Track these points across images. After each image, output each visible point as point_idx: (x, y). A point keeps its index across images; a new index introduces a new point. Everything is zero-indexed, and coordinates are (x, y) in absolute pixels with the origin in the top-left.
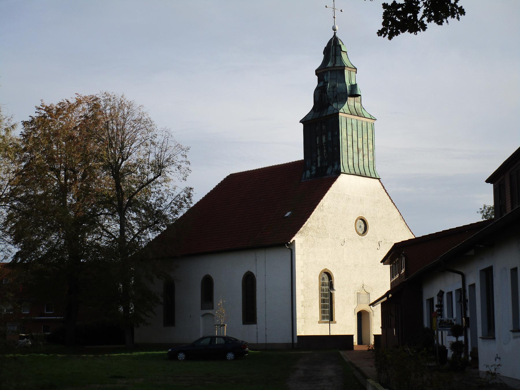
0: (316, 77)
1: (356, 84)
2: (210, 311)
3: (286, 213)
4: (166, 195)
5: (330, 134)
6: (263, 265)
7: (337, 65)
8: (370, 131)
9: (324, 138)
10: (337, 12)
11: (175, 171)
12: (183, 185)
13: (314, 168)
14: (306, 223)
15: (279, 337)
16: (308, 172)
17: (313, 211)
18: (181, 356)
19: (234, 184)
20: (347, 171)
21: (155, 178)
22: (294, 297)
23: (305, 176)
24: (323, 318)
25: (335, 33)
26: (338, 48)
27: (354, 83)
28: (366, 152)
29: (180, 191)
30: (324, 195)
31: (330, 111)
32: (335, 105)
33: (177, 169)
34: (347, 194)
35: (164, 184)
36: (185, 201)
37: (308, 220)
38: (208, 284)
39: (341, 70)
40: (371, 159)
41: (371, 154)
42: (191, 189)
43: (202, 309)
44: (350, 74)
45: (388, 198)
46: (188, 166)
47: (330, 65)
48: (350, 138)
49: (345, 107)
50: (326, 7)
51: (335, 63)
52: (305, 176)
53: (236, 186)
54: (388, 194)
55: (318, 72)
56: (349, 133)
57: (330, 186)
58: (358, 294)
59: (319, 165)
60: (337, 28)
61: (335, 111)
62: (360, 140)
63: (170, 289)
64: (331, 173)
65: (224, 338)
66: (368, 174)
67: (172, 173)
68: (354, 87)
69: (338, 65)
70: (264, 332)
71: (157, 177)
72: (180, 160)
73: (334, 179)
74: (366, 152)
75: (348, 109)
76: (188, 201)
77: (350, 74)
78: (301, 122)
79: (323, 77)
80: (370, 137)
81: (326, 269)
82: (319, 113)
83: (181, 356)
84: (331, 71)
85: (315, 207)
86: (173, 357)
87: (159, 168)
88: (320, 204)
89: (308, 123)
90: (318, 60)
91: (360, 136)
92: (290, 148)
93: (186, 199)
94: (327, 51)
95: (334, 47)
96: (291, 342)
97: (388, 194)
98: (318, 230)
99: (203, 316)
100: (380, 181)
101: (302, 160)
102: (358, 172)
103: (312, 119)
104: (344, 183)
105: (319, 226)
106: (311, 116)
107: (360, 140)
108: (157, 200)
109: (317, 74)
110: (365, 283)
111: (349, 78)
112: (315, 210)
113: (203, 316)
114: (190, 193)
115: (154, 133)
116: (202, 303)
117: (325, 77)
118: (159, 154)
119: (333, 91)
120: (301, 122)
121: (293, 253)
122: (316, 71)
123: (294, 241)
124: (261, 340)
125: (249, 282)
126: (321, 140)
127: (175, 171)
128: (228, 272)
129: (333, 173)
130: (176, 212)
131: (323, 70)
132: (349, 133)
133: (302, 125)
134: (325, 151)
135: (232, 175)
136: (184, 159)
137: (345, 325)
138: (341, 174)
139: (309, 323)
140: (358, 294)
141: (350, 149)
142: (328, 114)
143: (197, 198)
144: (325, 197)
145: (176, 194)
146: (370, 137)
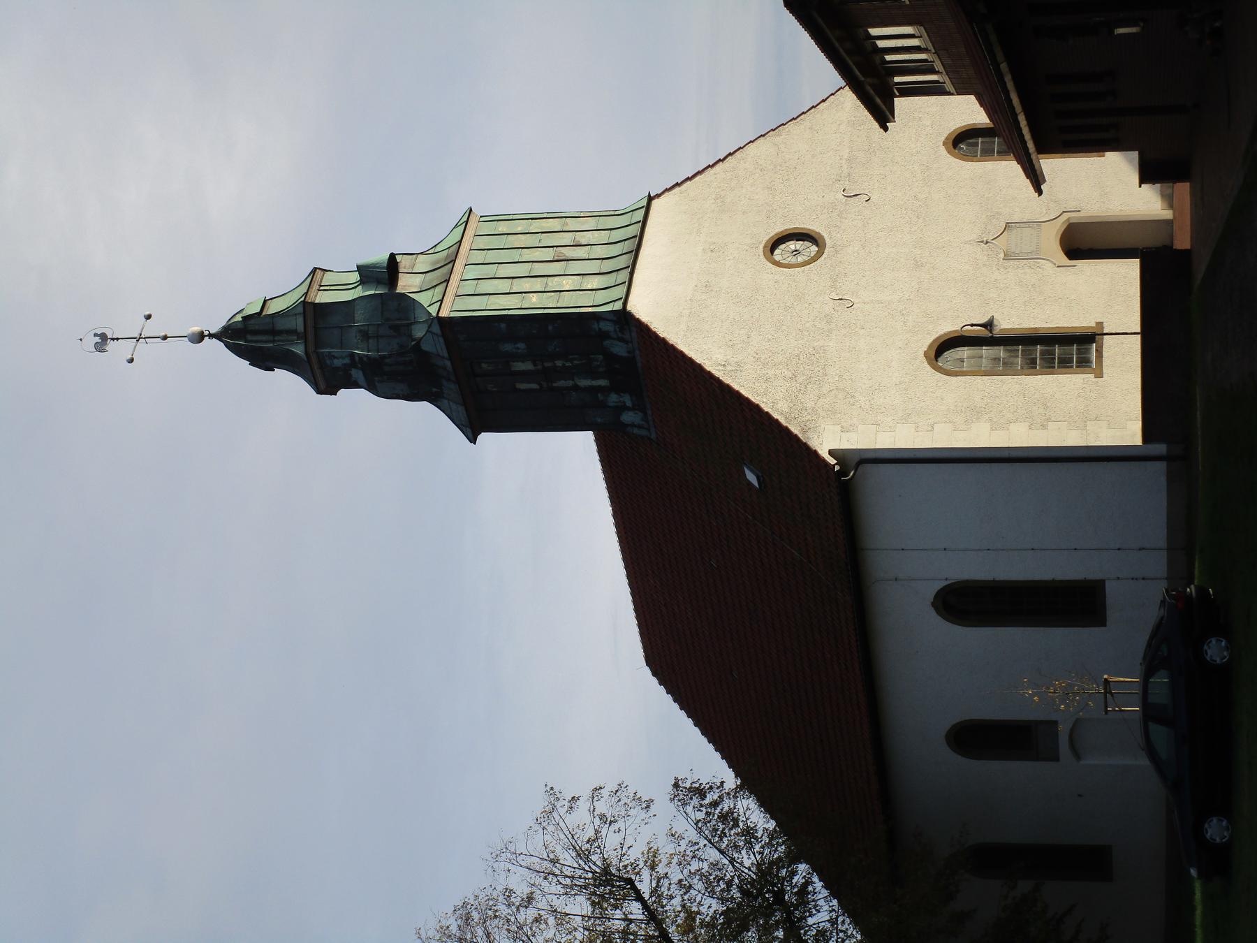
0: (342, 392)
2: (1063, 729)
3: (749, 483)
4: (695, 866)
5: (508, 347)
6: (913, 555)
7: (301, 328)
10: (152, 328)
11: (622, 834)
12: (665, 808)
13: (613, 398)
14: (776, 416)
15: (1149, 497)
16: (628, 417)
17: (738, 395)
18: (1215, 830)
19: (675, 650)
20: (620, 292)
21: (639, 898)
22: (1014, 454)
23: (640, 427)
24: (1084, 363)
25: (211, 336)
26: (253, 325)
27: (355, 277)
28: (567, 239)
29: (681, 819)
30: (690, 361)
31: (435, 346)
32: (419, 332)
33: (615, 826)
34: (695, 298)
35: (661, 869)
36: (715, 804)
37: (766, 408)
38: (975, 738)
39: (314, 315)
40: (590, 224)
41: (572, 224)
42: (676, 786)
43: (1057, 759)
46: (605, 792)
47: (299, 350)
49: (424, 299)
50: (131, 361)
52: (640, 427)
53: (686, 644)
54: (699, 173)
56: (504, 286)
57: (664, 341)
58: (1008, 256)
59: (603, 382)
60: (196, 329)
61: (436, 329)
63: (992, 859)
64: (626, 342)
65: (1149, 672)
66: (635, 230)
67: (630, 842)
68: (367, 274)
69: (299, 324)
70: (1132, 561)
71: (637, 892)
72: (587, 818)
73: (643, 330)
74: (567, 239)
75: (430, 293)
76: (716, 797)
79: (337, 369)
80: (520, 226)
81: (926, 354)
83: (1215, 830)
84: (318, 344)
85: (728, 389)
86: (1217, 862)
87: (609, 884)
88: (717, 374)
90: (286, 382)
91: (515, 255)
93: (707, 801)
94: (263, 358)
95: (249, 337)
96: (1162, 466)
97: (699, 173)
98: (801, 379)
99: (1077, 755)
100: (658, 196)
101: (598, 441)
102: (624, 261)
104: (659, 301)
105: (789, 374)
106: (454, 406)
108: (712, 894)
109: (332, 391)
110: (974, 237)
111: (342, 289)
112: (736, 387)
113: (1077, 755)
114: (690, 790)
115: (501, 898)
116: (1037, 759)
117: (337, 363)
118: (568, 881)
119: (378, 337)
121: (872, 456)
122: (319, 392)
123: (831, 453)
124: (1157, 565)
125: (966, 603)
126: (524, 375)
127: (622, 834)
128: (937, 672)
129: (627, 336)
130: (749, 833)
131: (316, 367)
132: (504, 286)
133: (484, 437)
134: (559, 363)
135: (650, 661)
136: (583, 805)
137: (1110, 296)
138: (629, 308)
139: (1104, 408)
140: (1008, 256)
141: (554, 284)
142: (446, 355)
143: (714, 769)
144: (698, 359)
145: (692, 834)
146: (520, 226)
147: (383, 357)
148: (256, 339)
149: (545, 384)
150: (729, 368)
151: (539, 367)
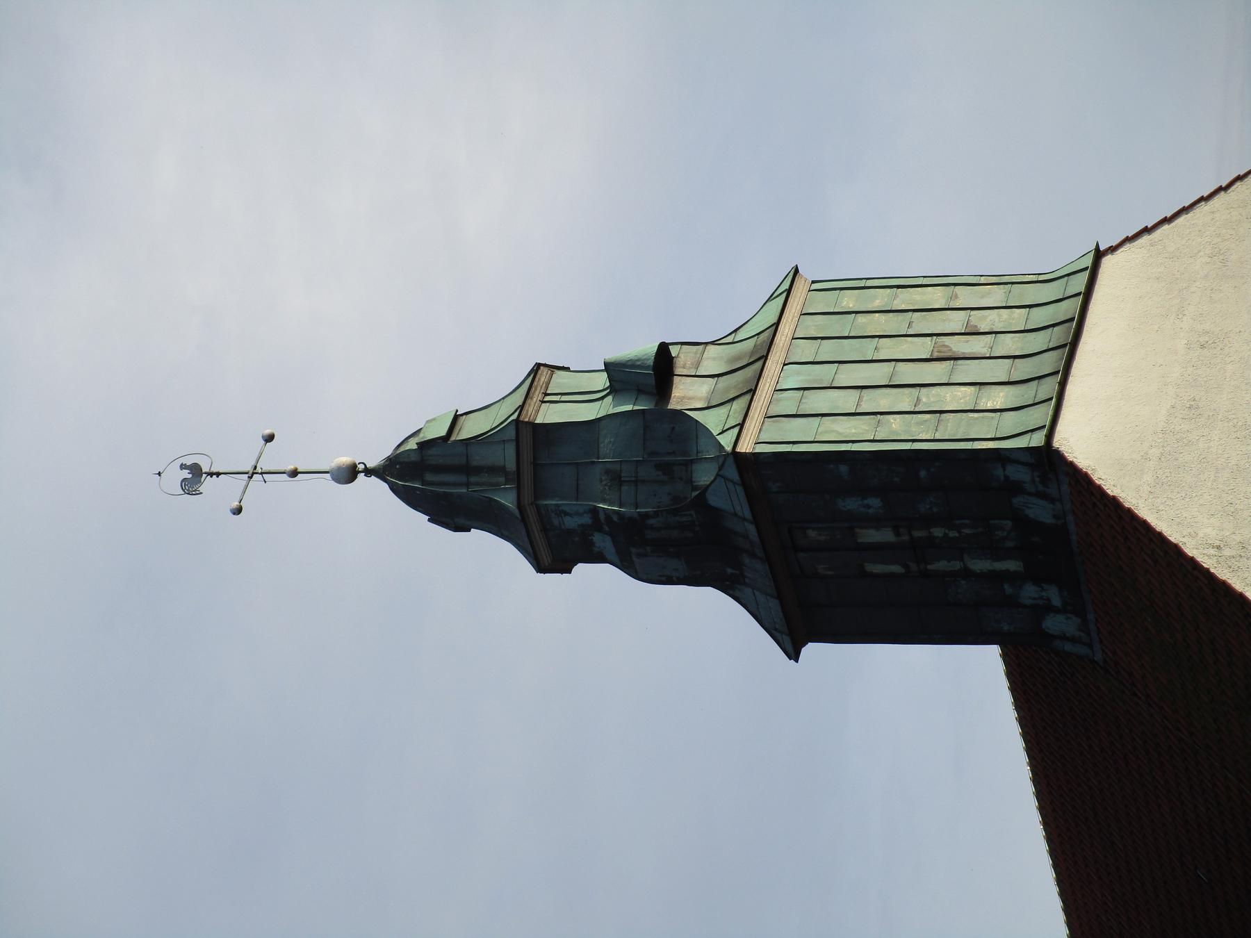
1: (610, 367)
5: (851, 504)
7: (511, 465)
8: (849, 301)
9: (871, 536)
13: (1029, 592)
16: (1053, 624)
20: (1041, 415)
23: (1074, 640)
25: (369, 472)
27: (602, 381)
28: (955, 321)
30: (1159, 539)
31: (729, 500)
32: (704, 475)
40: (996, 296)
41: (966, 297)
44: (567, 397)
45: (1204, 208)
47: (507, 500)
48: (872, 401)
49: (712, 421)
50: (238, 511)
51: (501, 470)
52: (1074, 640)
55: (553, 554)
56: (847, 401)
57: (1114, 502)
59: (1012, 565)
60: (345, 460)
61: (732, 472)
62: (889, 349)
66: (1070, 308)
68: (621, 376)
73: (1080, 481)
74: (955, 321)
75: (723, 411)
77: (567, 397)
78: (794, 655)
80: (879, 299)
82: (747, 560)
88: (1207, 563)
89: (797, 622)
90: (490, 556)
91: (867, 349)
92: (941, 720)
94: (451, 512)
100: (1113, 249)
101: (1005, 656)
102: (1049, 362)
103: (780, 597)
106: (761, 598)
107: (889, 349)
109: (564, 567)
111: (578, 405)
117: (571, 523)
119: (636, 482)
120: (794, 655)
122: (541, 568)
132: (847, 401)
133: (811, 650)
134: (938, 532)
138: (1057, 443)
141: (930, 399)
142: (748, 515)
144: (1173, 536)
147: (646, 516)
148: (440, 479)
149: (913, 566)
150: (1227, 552)
151: (905, 538)
